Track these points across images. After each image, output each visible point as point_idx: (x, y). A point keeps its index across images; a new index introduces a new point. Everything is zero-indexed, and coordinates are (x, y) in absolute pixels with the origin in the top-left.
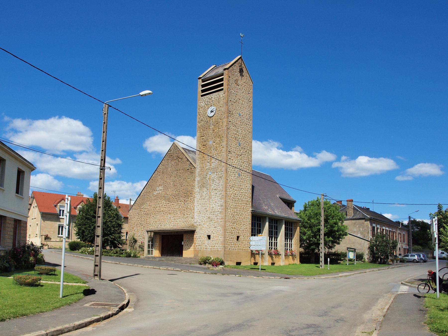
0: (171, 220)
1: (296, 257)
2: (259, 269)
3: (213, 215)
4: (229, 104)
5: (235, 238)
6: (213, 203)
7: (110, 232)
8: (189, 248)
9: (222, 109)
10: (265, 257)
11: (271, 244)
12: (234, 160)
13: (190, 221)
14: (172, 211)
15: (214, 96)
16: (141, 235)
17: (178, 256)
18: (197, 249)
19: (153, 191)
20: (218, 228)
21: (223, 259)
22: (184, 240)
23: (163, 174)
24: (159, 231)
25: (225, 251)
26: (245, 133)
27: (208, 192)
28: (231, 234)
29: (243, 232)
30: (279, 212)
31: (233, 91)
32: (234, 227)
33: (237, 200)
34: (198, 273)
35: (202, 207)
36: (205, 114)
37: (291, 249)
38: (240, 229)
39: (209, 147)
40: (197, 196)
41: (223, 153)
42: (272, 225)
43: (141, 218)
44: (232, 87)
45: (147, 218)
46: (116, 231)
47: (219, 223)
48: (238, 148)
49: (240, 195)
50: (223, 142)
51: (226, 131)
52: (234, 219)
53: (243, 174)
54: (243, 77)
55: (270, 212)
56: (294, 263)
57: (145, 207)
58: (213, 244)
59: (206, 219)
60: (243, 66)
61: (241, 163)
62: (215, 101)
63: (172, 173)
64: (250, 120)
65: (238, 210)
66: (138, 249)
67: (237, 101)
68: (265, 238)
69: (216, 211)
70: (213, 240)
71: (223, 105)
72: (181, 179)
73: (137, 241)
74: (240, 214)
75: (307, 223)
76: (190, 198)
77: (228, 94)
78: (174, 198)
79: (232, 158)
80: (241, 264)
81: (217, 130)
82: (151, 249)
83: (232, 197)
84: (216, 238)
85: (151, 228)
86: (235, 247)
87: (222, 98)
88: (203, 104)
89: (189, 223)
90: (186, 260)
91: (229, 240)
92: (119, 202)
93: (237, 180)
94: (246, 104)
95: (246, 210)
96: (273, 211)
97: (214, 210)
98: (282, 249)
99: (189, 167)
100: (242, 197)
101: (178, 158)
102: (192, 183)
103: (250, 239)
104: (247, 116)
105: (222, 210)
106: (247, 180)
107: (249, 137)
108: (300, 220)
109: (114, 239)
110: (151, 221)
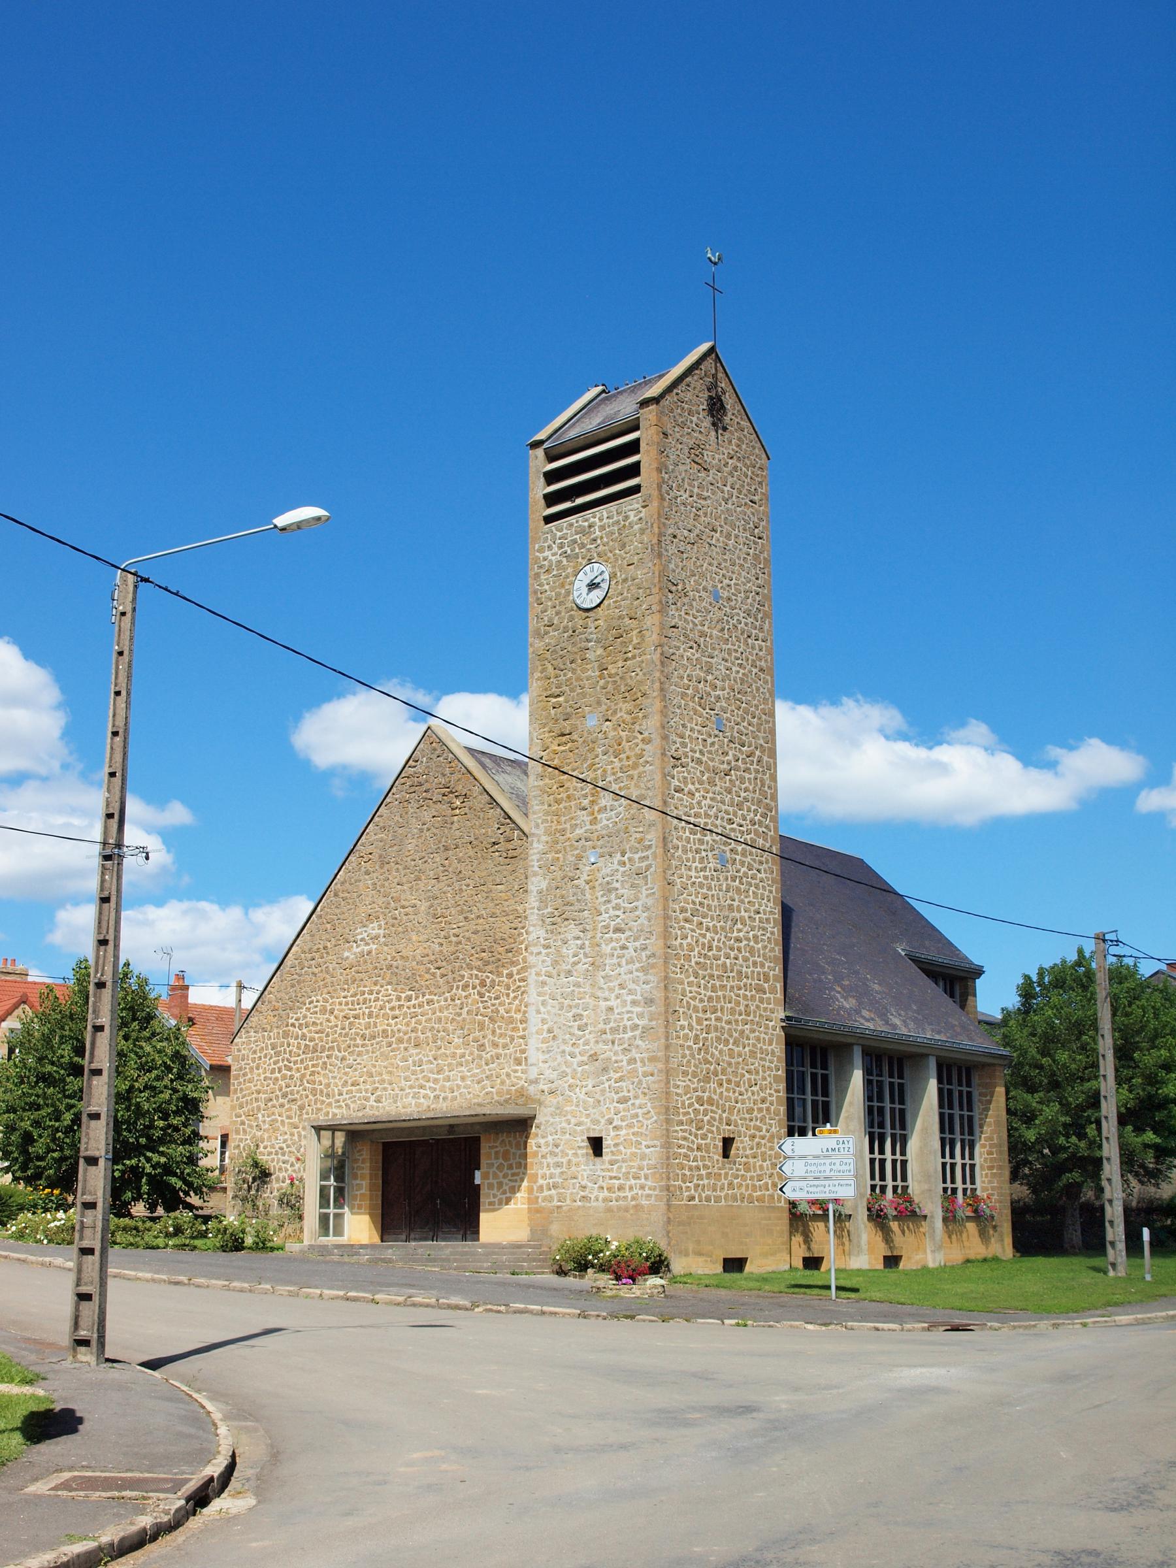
1: (995, 1227)
3: (613, 1043)
4: (667, 551)
5: (715, 1146)
6: (611, 990)
10: (851, 1229)
11: (877, 1168)
12: (697, 794)
13: (508, 1075)
14: (429, 1034)
15: (601, 520)
16: (288, 1146)
17: (456, 1240)
21: (663, 1244)
22: (484, 1162)
25: (669, 1206)
26: (743, 674)
27: (587, 943)
28: (694, 1130)
29: (747, 1116)
31: (682, 493)
33: (716, 973)
35: (561, 1009)
39: (584, 742)
40: (538, 962)
41: (648, 767)
43: (290, 1069)
44: (680, 478)
45: (313, 1066)
46: (176, 1129)
47: (640, 1082)
48: (713, 744)
50: (645, 717)
52: (707, 1062)
53: (738, 857)
54: (727, 435)
55: (868, 1023)
56: (990, 1256)
58: (615, 1178)
59: (581, 1064)
60: (723, 385)
61: (731, 809)
62: (605, 540)
64: (760, 616)
65: (725, 1018)
67: (703, 538)
68: (851, 1142)
70: (616, 1161)
71: (640, 556)
72: (464, 887)
74: (731, 1036)
76: (505, 972)
77: (661, 507)
78: (434, 975)
79: (690, 786)
80: (748, 1268)
81: (620, 664)
82: (335, 1208)
84: (629, 1151)
87: (636, 527)
88: (552, 556)
89: (503, 1083)
92: (186, 997)
93: (713, 883)
94: (741, 546)
96: (883, 1016)
100: (741, 961)
101: (451, 792)
103: (780, 1148)
104: (749, 601)
105: (650, 1020)
106: (758, 881)
107: (762, 690)
109: (168, 1170)
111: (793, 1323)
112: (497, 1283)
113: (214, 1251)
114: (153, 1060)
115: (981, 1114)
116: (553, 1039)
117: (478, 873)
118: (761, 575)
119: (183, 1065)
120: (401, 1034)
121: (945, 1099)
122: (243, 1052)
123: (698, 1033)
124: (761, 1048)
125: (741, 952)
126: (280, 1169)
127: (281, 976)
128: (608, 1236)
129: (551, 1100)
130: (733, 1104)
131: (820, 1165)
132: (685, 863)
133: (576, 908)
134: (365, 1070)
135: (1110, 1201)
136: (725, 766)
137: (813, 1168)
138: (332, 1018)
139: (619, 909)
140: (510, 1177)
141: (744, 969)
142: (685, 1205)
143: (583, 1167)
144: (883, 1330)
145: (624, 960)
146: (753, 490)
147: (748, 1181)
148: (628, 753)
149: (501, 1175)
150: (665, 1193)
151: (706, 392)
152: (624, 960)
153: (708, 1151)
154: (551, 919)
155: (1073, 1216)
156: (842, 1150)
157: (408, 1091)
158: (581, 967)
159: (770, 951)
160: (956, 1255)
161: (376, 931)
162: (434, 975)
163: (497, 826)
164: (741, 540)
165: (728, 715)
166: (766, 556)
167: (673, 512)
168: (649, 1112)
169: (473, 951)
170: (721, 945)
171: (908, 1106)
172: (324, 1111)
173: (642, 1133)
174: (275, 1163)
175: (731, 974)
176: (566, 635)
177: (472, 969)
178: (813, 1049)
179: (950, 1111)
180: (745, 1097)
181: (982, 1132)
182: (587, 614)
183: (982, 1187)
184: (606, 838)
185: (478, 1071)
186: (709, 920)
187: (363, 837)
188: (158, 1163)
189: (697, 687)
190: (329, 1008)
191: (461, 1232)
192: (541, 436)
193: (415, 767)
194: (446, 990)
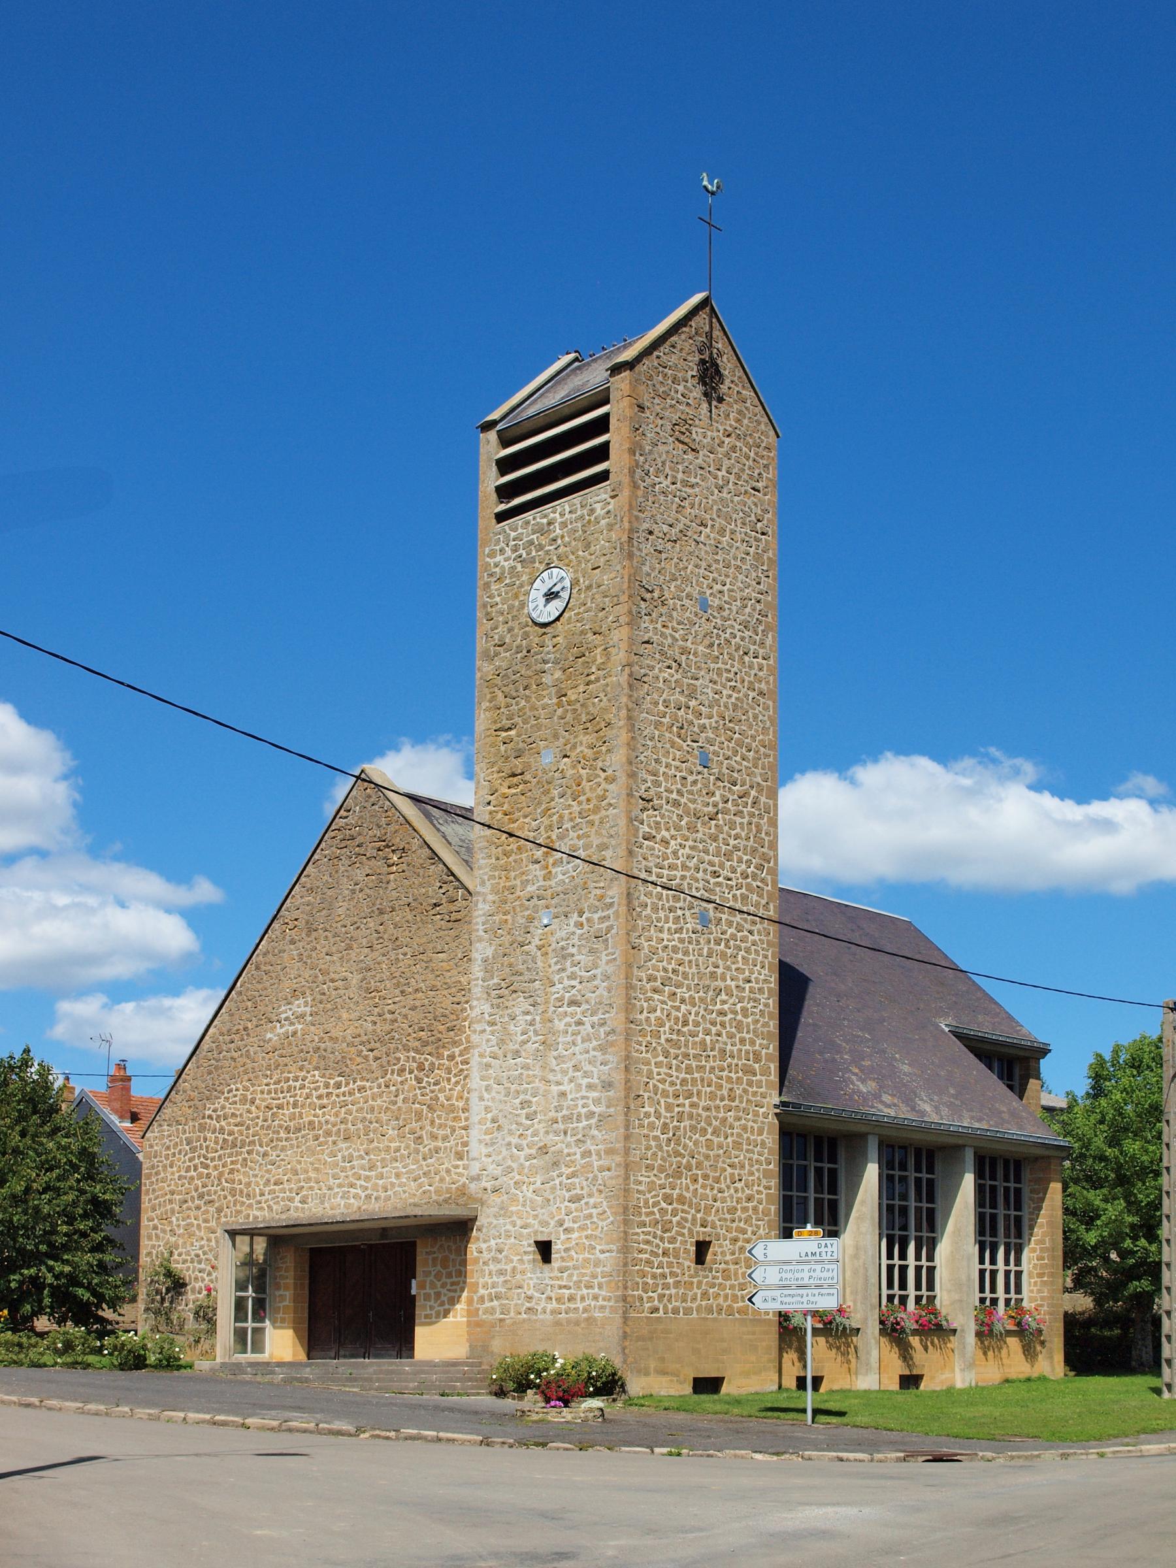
0: (353, 1168)
1: (1042, 1343)
2: (804, 1411)
3: (565, 1133)
4: (640, 550)
5: (686, 1251)
6: (564, 1072)
7: (51, 1245)
8: (446, 1314)
10: (860, 1345)
11: (896, 1277)
12: (673, 842)
13: (448, 1171)
14: (360, 1126)
15: (562, 515)
16: (205, 1253)
17: (390, 1357)
18: (484, 1314)
19: (262, 1022)
20: (592, 1201)
21: (617, 1362)
22: (420, 1270)
23: (308, 935)
25: (625, 1319)
26: (737, 699)
27: (538, 1018)
28: (659, 1233)
29: (728, 1216)
31: (662, 479)
32: (676, 1192)
33: (692, 1052)
34: (449, 1440)
35: (508, 1094)
38: (715, 1201)
39: (538, 782)
41: (611, 811)
42: (995, 1186)
43: (207, 1167)
45: (232, 1163)
46: (84, 1235)
47: (595, 1178)
48: (695, 782)
49: (713, 1023)
50: (609, 751)
51: (626, 691)
52: (678, 1154)
54: (723, 407)
56: (1035, 1375)
57: (223, 1108)
58: (565, 1287)
59: (529, 1158)
60: (720, 346)
61: (716, 860)
62: (567, 539)
63: (358, 928)
64: (761, 628)
65: (702, 1104)
66: (191, 1324)
67: (689, 534)
69: (579, 1115)
70: (567, 1269)
71: (607, 558)
72: (401, 957)
73: (184, 1285)
74: (710, 1124)
75: (1102, 1158)
76: (446, 1053)
77: (633, 496)
79: (664, 833)
80: (725, 1389)
81: (581, 689)
82: (253, 1321)
83: (663, 1037)
84: (581, 1257)
85: (256, 1217)
87: (603, 522)
88: (504, 561)
89: (442, 1180)
91: (648, 1262)
92: (128, 1089)
93: (691, 947)
94: (738, 544)
95: (744, 1104)
96: (909, 1101)
97: (568, 1108)
98: (961, 1301)
99: (442, 891)
100: (724, 1038)
101: (388, 846)
102: (455, 972)
104: (748, 610)
105: (608, 1107)
106: (749, 945)
107: (761, 717)
109: (73, 1280)
111: (737, 1452)
112: (406, 1406)
113: (110, 1369)
114: (54, 1157)
115: (1031, 1213)
117: (416, 939)
118: (764, 579)
119: (92, 1164)
120: (329, 1126)
122: (156, 1148)
123: (668, 1121)
124: (748, 1138)
125: (725, 1028)
127: (197, 1061)
128: (556, 1353)
129: (495, 1199)
130: (711, 1202)
131: (798, 1271)
132: (655, 923)
133: (526, 978)
134: (289, 1166)
136: (710, 809)
137: (789, 1275)
138: (253, 1108)
139: (575, 979)
140: (448, 1287)
141: (729, 1047)
142: (647, 1317)
143: (529, 1275)
144: (848, 1460)
145: (579, 1038)
146: (756, 475)
147: (727, 1291)
148: (589, 795)
149: (439, 1284)
150: (621, 1305)
151: (697, 354)
152: (579, 1038)
153: (677, 1257)
154: (497, 992)
156: (824, 1254)
157: (336, 1190)
159: (763, 1026)
160: (990, 1372)
161: (303, 1009)
162: (366, 1058)
163: (439, 884)
164: (739, 537)
165: (716, 748)
166: (771, 555)
167: (650, 503)
169: (410, 1030)
171: (939, 1205)
172: (245, 1213)
173: (596, 1237)
174: (190, 1272)
175: (712, 1053)
176: (519, 656)
179: (930, 1205)
180: (726, 1194)
181: (1031, 1235)
182: (544, 630)
183: (1030, 1298)
184: (562, 895)
185: (414, 1167)
186: (684, 990)
188: (62, 1273)
189: (676, 715)
190: (249, 1097)
191: (397, 1349)
193: (346, 817)
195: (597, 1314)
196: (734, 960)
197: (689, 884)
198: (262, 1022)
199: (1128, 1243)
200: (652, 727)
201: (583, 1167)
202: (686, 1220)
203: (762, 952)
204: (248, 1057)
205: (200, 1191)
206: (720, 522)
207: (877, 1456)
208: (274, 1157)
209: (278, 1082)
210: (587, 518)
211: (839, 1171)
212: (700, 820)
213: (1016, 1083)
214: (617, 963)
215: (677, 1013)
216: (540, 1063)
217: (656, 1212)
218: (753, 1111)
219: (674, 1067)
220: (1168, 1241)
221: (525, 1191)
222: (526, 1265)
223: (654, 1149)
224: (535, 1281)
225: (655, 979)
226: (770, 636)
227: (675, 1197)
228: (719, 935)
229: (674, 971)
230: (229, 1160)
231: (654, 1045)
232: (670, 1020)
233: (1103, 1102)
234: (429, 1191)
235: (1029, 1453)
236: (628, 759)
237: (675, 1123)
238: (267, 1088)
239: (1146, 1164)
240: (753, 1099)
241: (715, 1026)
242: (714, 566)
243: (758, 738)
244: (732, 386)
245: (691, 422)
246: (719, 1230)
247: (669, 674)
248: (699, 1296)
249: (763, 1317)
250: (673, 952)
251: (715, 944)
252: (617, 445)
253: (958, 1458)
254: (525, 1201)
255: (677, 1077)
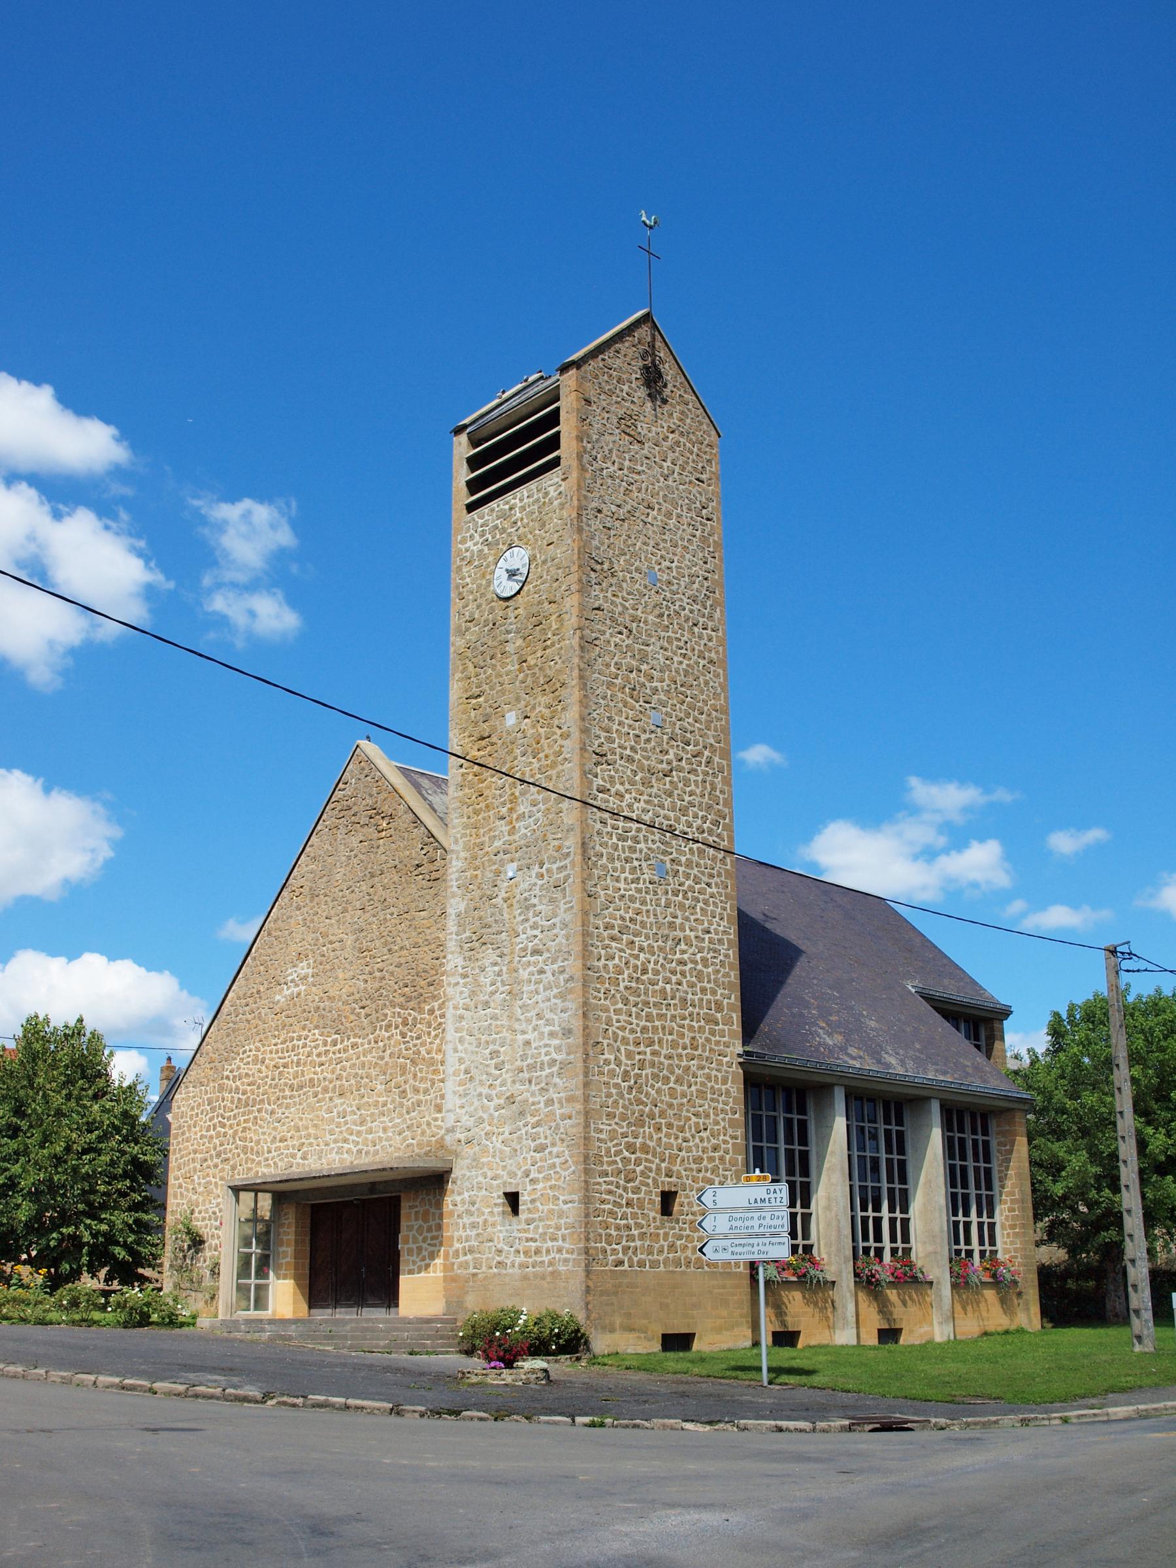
1: (1019, 1294)
2: (759, 1369)
3: (530, 1082)
4: (589, 525)
6: (529, 1021)
7: (90, 1204)
9: (558, 551)
12: (627, 796)
14: (353, 1082)
15: (521, 500)
18: (459, 1268)
19: (272, 985)
20: (555, 1150)
21: (581, 1317)
23: (311, 901)
24: (280, 1182)
25: (588, 1273)
26: (688, 665)
27: (504, 969)
28: (622, 1182)
29: (694, 1166)
30: (907, 1061)
31: (609, 464)
33: (652, 1000)
34: (357, 1408)
36: (483, 591)
37: (991, 1251)
39: (503, 743)
40: (455, 992)
41: (567, 765)
43: (224, 1126)
44: (606, 449)
45: (245, 1121)
47: (557, 1127)
48: (648, 740)
49: (674, 972)
52: (640, 1102)
53: (681, 869)
54: (667, 408)
55: (856, 1061)
56: (1013, 1327)
57: (239, 1068)
58: (531, 1239)
61: (672, 814)
62: (525, 521)
64: (709, 603)
65: (664, 1052)
67: (637, 514)
69: (542, 1064)
72: (389, 916)
74: (672, 1073)
75: (1063, 1111)
76: (427, 1008)
77: (581, 479)
78: (358, 1015)
79: (618, 786)
80: (696, 1346)
82: (257, 1278)
84: (546, 1208)
85: (264, 1174)
86: (650, 1253)
87: (556, 503)
89: (423, 1133)
90: (397, 1329)
93: (648, 897)
94: (685, 527)
95: (707, 1053)
96: (876, 1054)
97: (532, 1056)
99: (423, 852)
102: (434, 929)
103: (699, 1199)
104: (696, 586)
105: (568, 1054)
106: (707, 897)
107: (711, 684)
108: (1024, 1096)
109: (110, 1239)
110: (262, 1137)
111: (666, 1421)
115: (1000, 1165)
116: (470, 1080)
118: (710, 559)
119: (133, 1126)
120: (327, 1083)
121: (952, 1148)
122: (183, 1109)
123: (628, 1069)
124: (712, 1087)
125: (686, 977)
126: (213, 1236)
127: (219, 1025)
129: (468, 1151)
132: (611, 872)
133: (494, 930)
134: (292, 1123)
135: (1133, 1261)
136: (664, 766)
137: (739, 1224)
138: (263, 1068)
141: (690, 996)
142: (610, 1270)
143: (499, 1228)
145: (541, 986)
146: (699, 467)
147: (695, 1243)
149: (420, 1238)
150: (583, 1257)
152: (541, 986)
153: (641, 1208)
154: (469, 945)
155: (1115, 1280)
156: (773, 1200)
157: (332, 1145)
158: (499, 997)
159: (723, 976)
160: (969, 1326)
161: (306, 971)
163: (420, 846)
165: (669, 709)
166: (716, 539)
167: (598, 485)
168: (567, 1161)
170: (659, 967)
171: (910, 1157)
173: (559, 1187)
174: (208, 1229)
175: (672, 1002)
176: (486, 629)
177: (394, 1007)
178: (788, 1091)
180: (691, 1144)
181: (1003, 1187)
182: (507, 604)
184: (524, 848)
185: (399, 1121)
187: (295, 870)
189: (628, 677)
190: (260, 1057)
192: (466, 421)
193: (344, 789)
194: (369, 1032)
195: (562, 1268)
196: (692, 911)
197: (644, 836)
198: (272, 985)
199: (1093, 1194)
200: (605, 687)
201: (547, 1116)
202: (650, 1170)
203: (720, 905)
204: (260, 1018)
205: (218, 1149)
206: (666, 506)
207: (821, 1425)
208: (280, 1115)
209: (284, 1042)
210: (542, 500)
211: (809, 1122)
212: (654, 776)
213: (983, 1043)
214: (574, 911)
215: (636, 961)
216: (507, 1013)
217: (619, 1161)
218: (717, 1060)
219: (634, 1015)
220: (1127, 1186)
221: (495, 1142)
222: (496, 1218)
223: (615, 1097)
224: (505, 1234)
225: (613, 927)
226: (718, 610)
227: (638, 1145)
228: (677, 886)
229: (631, 920)
230: (242, 1119)
231: (613, 992)
232: (628, 967)
233: (1061, 1054)
234: (412, 1144)
235: (986, 1419)
236: (580, 715)
237: (636, 1071)
238: (275, 1048)
239: (1105, 1115)
240: (716, 1048)
241: (676, 975)
242: (662, 545)
243: (709, 703)
244: (675, 390)
245: (636, 418)
246: (685, 1180)
247: (620, 639)
248: (666, 1248)
249: (734, 1270)
250: (630, 901)
251: (673, 895)
252: (567, 434)
253: (909, 1425)
254: (494, 1152)
255: (638, 1025)
